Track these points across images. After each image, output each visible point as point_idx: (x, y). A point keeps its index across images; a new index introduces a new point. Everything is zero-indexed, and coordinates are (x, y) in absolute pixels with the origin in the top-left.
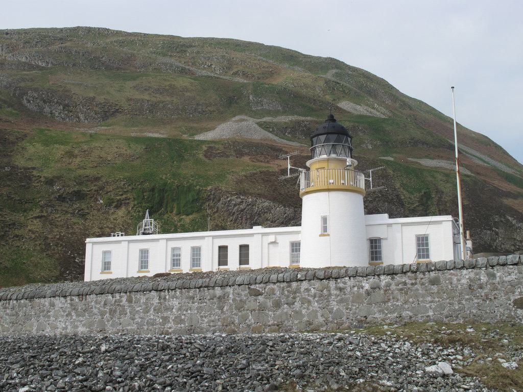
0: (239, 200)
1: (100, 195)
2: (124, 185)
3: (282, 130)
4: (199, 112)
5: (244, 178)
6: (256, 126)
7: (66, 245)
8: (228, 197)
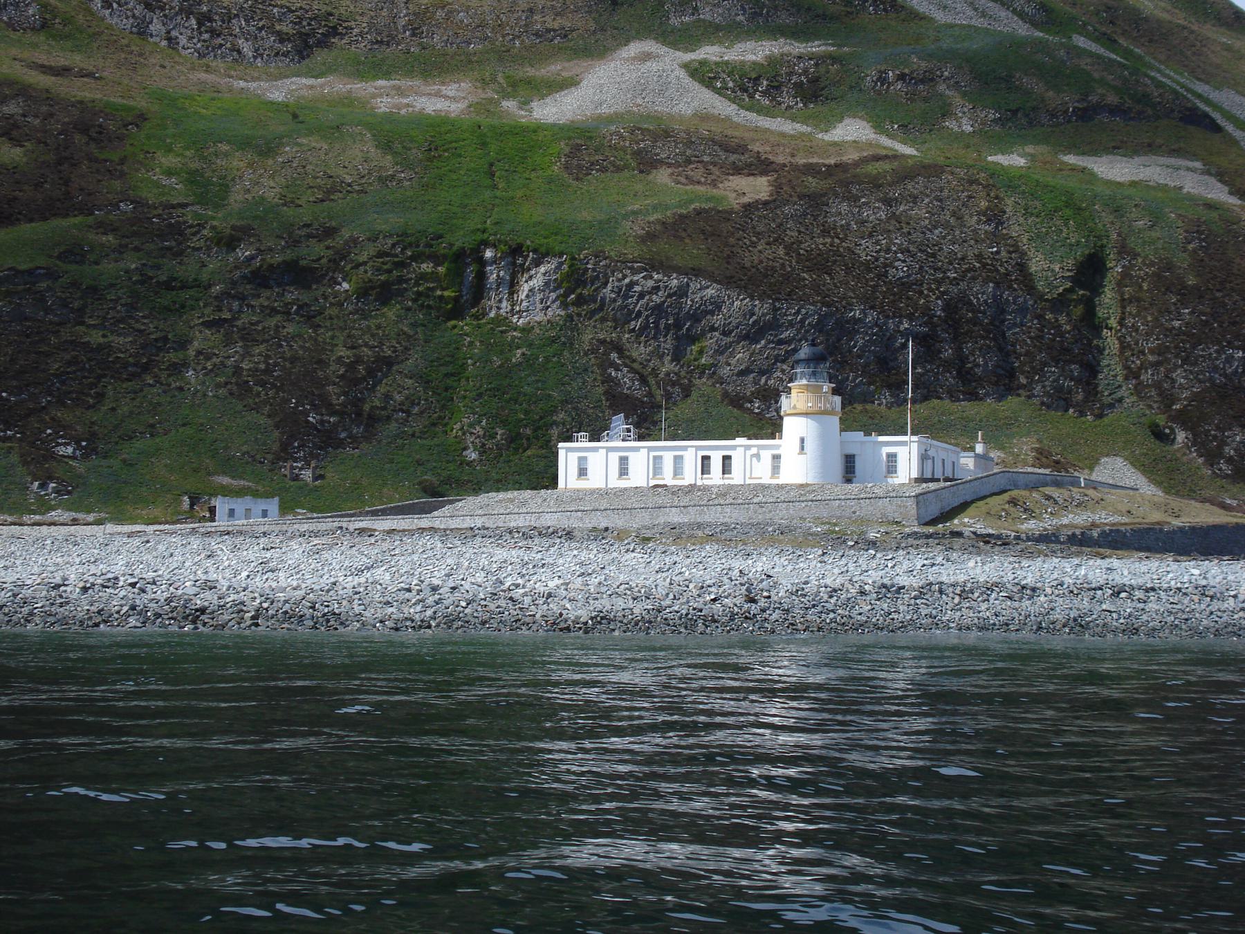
0: (650, 283)
1: (342, 270)
2: (394, 245)
3: (745, 84)
4: (537, 35)
5: (658, 227)
6: (682, 74)
7: (283, 384)
8: (625, 277)
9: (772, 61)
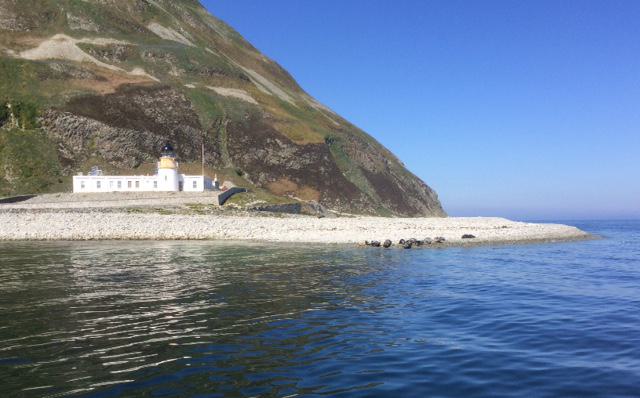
0: (73, 120)
3: (99, 52)
9: (109, 46)
